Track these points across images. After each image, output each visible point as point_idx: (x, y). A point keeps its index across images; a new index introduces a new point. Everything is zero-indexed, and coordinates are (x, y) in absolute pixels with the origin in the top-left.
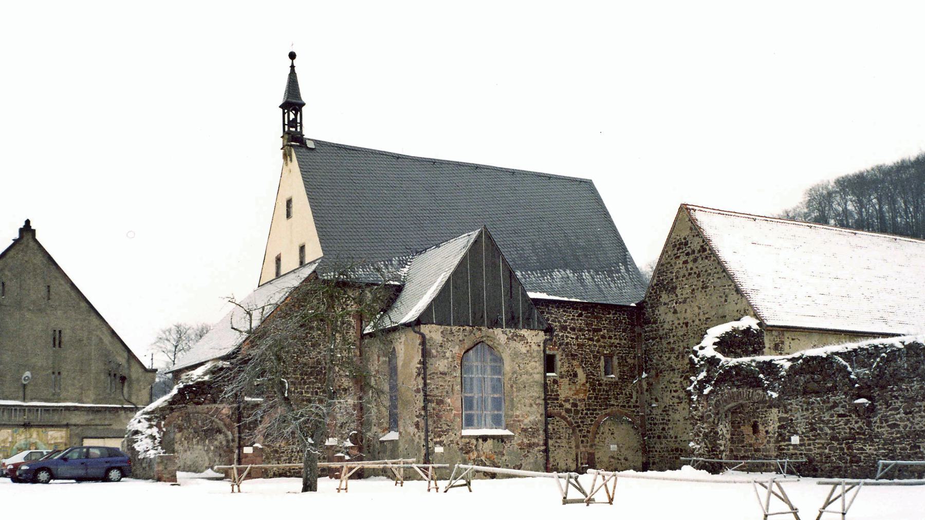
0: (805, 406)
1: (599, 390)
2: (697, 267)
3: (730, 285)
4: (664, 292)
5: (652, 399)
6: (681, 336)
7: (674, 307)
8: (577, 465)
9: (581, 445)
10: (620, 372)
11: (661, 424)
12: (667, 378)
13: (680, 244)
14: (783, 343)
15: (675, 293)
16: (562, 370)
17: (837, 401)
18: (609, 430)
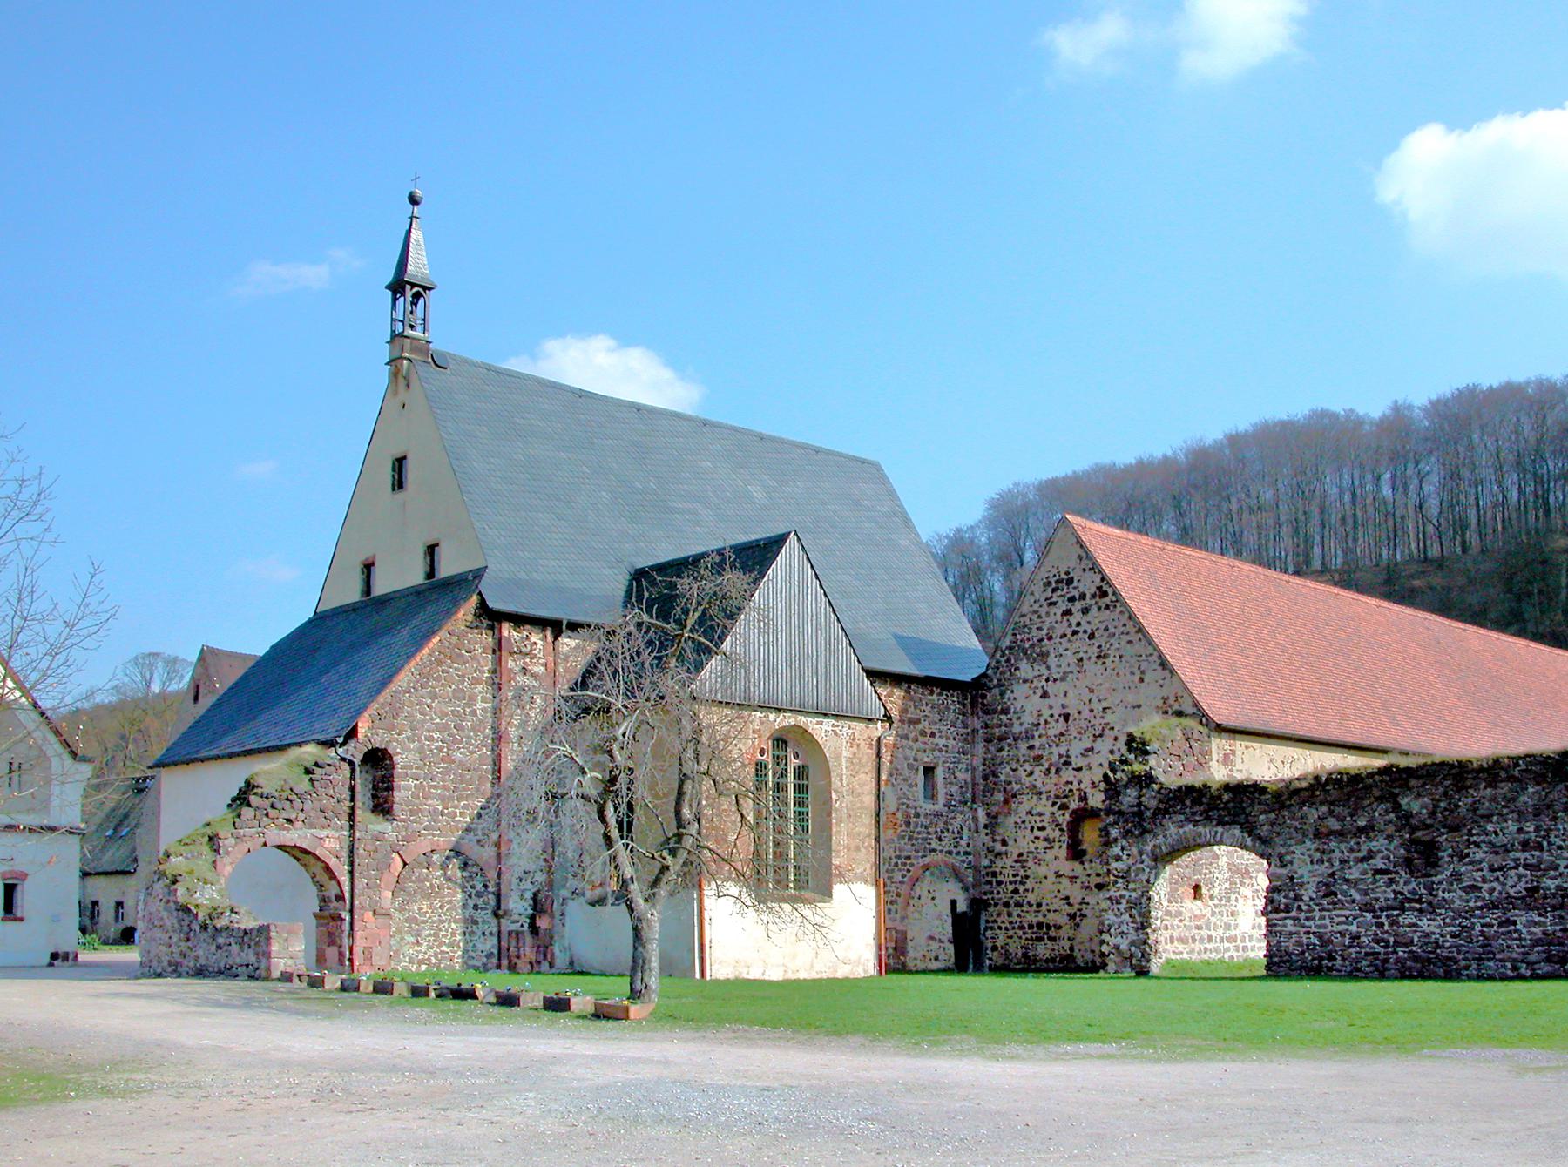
0: (1317, 856)
2: (1089, 622)
3: (1151, 655)
4: (1025, 661)
5: (994, 841)
6: (1055, 736)
7: (1043, 687)
10: (946, 793)
11: (1011, 883)
12: (1026, 806)
13: (1057, 582)
14: (1234, 752)
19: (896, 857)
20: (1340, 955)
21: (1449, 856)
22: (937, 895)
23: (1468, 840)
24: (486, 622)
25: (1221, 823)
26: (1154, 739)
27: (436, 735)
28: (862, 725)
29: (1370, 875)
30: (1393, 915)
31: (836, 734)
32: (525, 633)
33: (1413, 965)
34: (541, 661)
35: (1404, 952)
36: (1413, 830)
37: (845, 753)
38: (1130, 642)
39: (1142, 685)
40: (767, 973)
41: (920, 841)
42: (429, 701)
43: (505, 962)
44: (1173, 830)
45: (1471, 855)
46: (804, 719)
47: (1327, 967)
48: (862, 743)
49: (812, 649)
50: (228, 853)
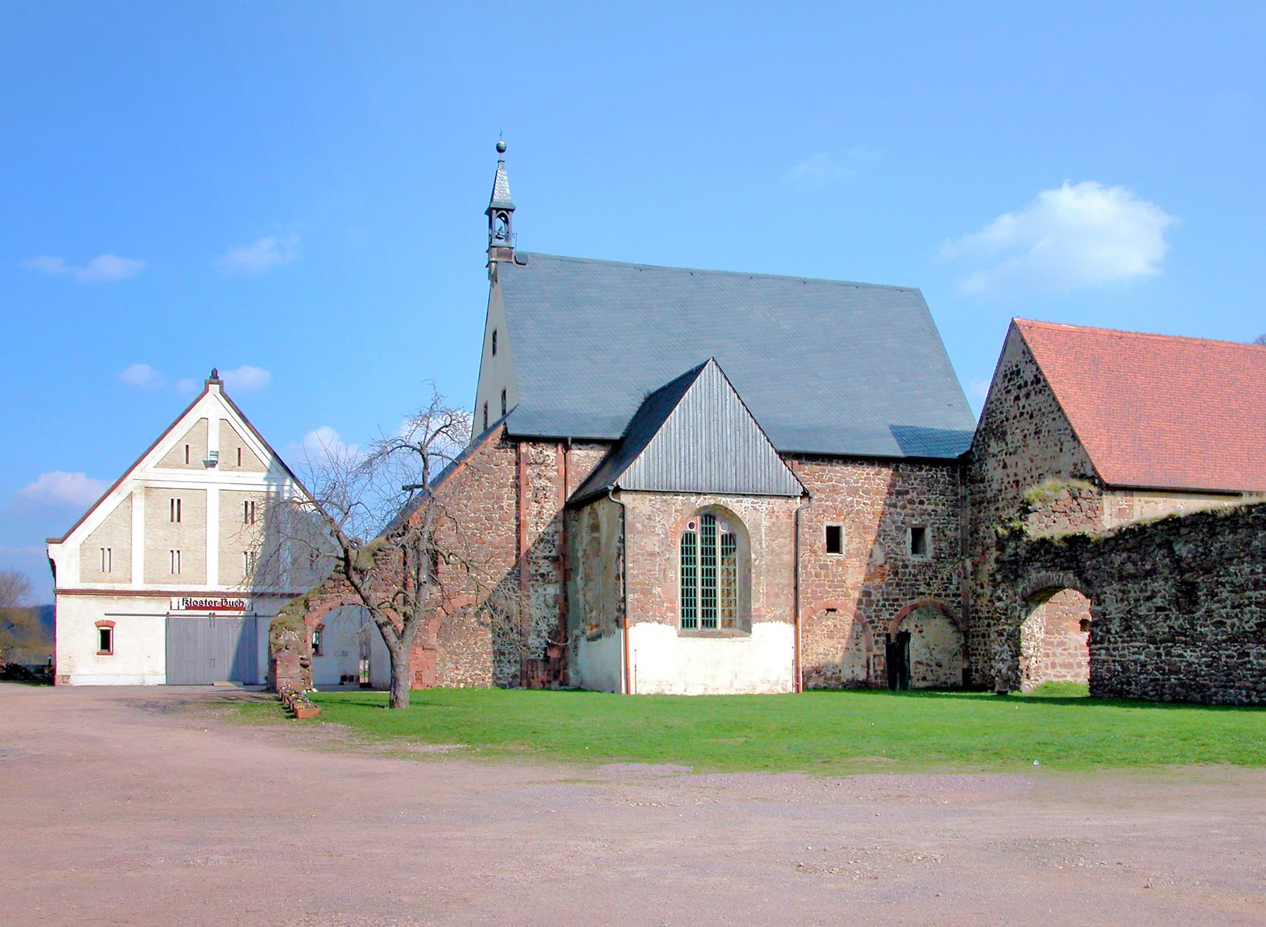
0: (1120, 595)
1: (905, 574)
4: (993, 439)
5: (977, 585)
6: (1011, 499)
7: (1003, 460)
8: (868, 673)
9: (875, 647)
11: (986, 618)
15: (1005, 440)
16: (851, 547)
17: (1156, 590)
18: (916, 626)
19: (883, 600)
20: (1134, 681)
21: (1205, 595)
22: (924, 628)
23: (1217, 581)
24: (510, 444)
25: (1063, 569)
26: (1037, 500)
27: (472, 525)
28: (782, 501)
29: (1153, 612)
30: (1168, 647)
31: (755, 509)
32: (540, 449)
33: (1181, 690)
34: (554, 468)
35: (1175, 679)
36: (1182, 573)
37: (764, 523)
38: (1054, 419)
39: (1062, 454)
40: (688, 690)
41: (908, 586)
42: (465, 502)
43: (525, 682)
44: (1036, 576)
45: (1219, 595)
46: (723, 499)
47: (1126, 691)
48: (782, 515)
49: (730, 444)
50: (315, 610)
